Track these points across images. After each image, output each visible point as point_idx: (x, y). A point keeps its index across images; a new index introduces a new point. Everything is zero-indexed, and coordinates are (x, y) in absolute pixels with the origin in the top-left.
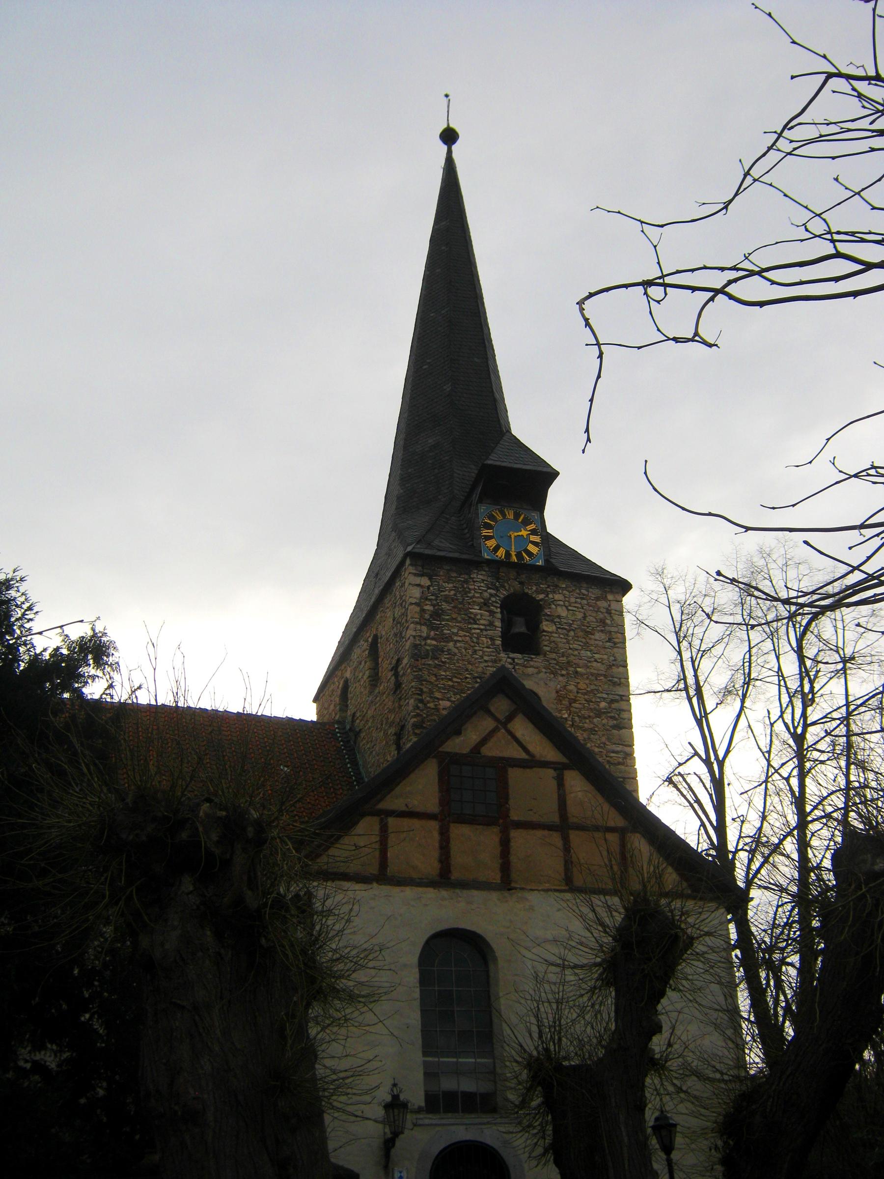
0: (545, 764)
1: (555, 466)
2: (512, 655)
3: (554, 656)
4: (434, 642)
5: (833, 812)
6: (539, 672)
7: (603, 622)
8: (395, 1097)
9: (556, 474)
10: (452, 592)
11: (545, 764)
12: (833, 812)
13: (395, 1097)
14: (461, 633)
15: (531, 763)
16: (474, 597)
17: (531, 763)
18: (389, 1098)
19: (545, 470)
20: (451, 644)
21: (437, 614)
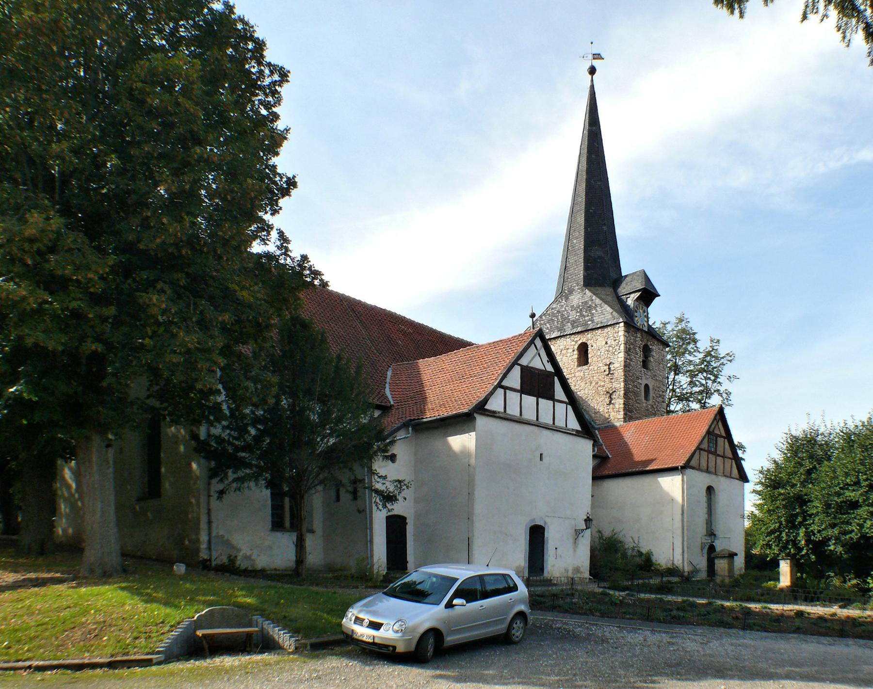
1: (659, 291)
15: (721, 436)
17: (721, 436)
21: (629, 349)
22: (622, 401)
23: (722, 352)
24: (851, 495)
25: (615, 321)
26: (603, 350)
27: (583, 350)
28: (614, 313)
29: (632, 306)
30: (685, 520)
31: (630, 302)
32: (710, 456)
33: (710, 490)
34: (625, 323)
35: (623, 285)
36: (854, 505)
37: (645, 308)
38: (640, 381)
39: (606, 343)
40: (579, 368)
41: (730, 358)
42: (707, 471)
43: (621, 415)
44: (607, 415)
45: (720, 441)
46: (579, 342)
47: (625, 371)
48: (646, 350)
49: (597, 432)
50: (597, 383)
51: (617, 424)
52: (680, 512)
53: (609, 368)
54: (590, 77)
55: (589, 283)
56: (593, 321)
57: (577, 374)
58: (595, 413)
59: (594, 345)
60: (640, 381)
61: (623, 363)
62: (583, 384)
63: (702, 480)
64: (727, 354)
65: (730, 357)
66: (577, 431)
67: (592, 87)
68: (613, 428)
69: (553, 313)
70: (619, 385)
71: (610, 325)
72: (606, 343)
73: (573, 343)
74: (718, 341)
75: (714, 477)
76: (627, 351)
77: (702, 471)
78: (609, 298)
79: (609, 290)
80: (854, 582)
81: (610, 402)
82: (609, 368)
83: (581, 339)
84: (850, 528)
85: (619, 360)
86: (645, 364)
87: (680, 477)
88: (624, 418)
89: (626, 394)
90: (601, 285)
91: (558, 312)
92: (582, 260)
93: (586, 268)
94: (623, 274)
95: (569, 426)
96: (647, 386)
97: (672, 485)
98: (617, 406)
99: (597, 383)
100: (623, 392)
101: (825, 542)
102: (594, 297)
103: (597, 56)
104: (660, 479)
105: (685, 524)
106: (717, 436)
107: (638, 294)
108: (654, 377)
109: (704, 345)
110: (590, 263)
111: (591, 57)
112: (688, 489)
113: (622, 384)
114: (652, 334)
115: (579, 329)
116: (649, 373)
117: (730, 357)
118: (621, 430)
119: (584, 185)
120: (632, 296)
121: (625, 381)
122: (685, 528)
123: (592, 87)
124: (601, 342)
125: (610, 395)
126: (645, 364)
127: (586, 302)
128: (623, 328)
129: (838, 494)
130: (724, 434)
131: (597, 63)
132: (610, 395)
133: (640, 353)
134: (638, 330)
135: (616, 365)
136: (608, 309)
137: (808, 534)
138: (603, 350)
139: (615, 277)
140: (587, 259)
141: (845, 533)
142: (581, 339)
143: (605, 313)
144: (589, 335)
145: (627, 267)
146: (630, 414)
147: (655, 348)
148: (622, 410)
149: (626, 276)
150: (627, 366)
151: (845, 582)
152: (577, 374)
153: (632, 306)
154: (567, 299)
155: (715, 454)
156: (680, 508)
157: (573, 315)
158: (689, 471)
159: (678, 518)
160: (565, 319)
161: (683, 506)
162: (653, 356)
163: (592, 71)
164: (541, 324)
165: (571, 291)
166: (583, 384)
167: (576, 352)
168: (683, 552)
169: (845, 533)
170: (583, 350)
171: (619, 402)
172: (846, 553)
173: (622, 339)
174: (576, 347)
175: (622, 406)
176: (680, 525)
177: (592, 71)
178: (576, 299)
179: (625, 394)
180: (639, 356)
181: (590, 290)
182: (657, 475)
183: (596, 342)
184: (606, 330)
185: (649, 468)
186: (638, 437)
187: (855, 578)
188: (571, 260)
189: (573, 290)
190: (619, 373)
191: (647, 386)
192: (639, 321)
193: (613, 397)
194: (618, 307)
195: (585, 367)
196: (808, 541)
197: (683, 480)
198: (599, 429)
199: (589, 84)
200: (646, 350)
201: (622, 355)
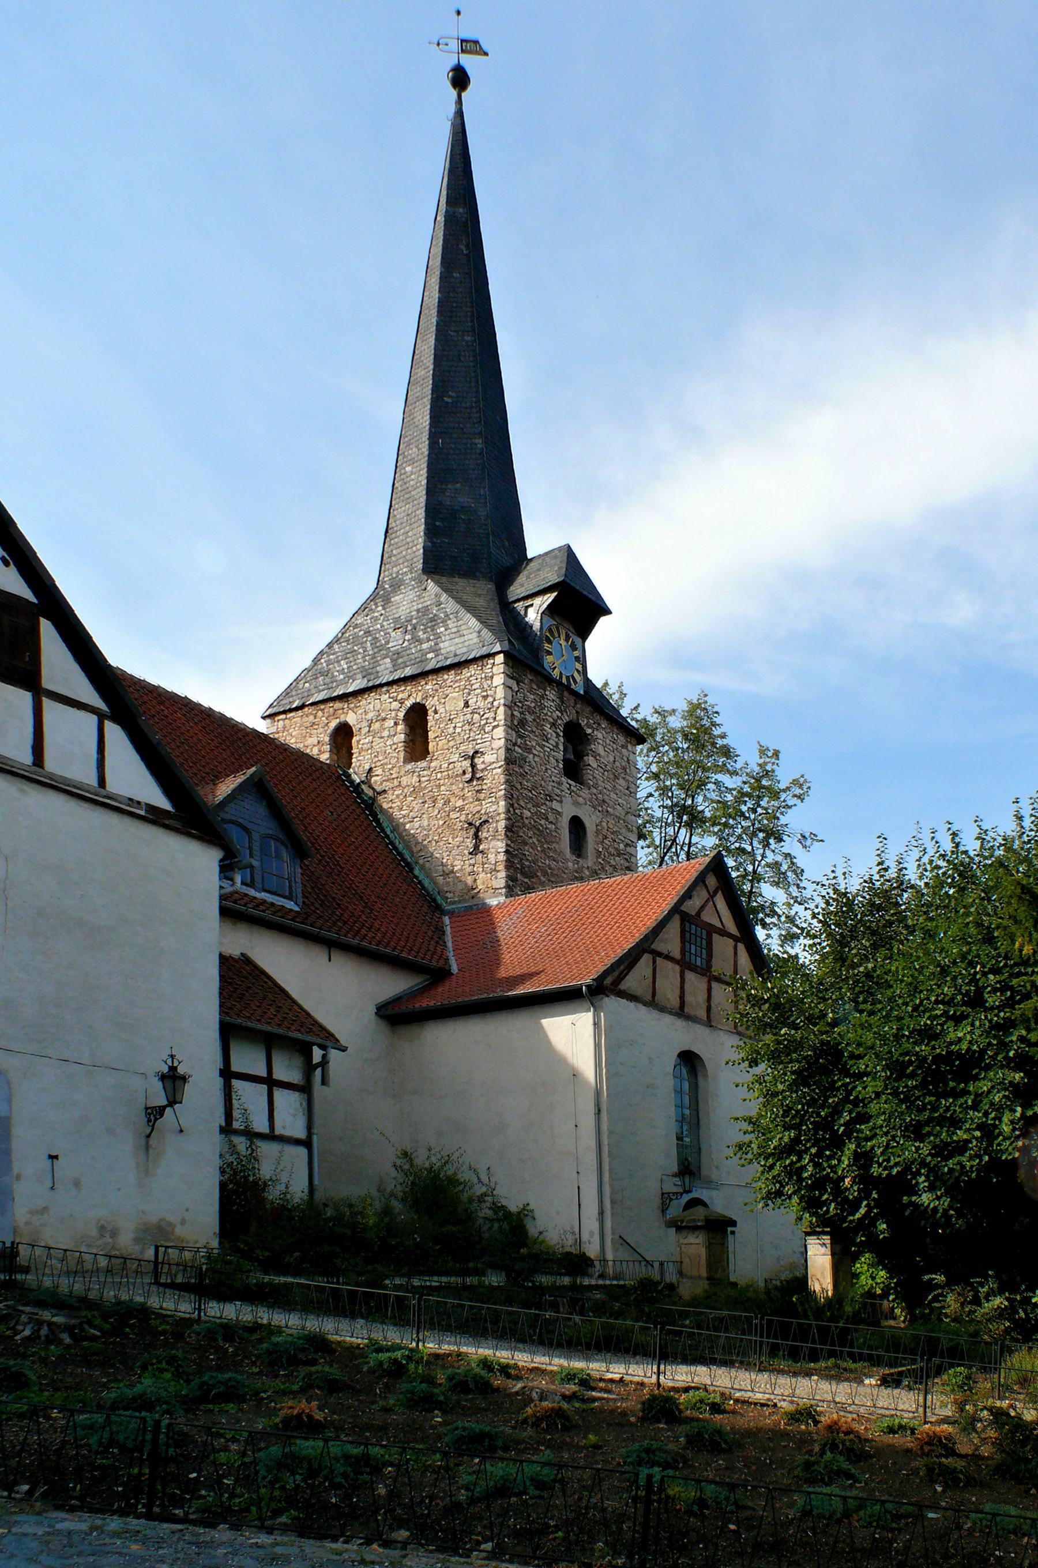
0: (730, 936)
1: (609, 601)
2: (570, 781)
3: (595, 791)
4: (520, 751)
5: (668, 957)
6: (586, 804)
7: (624, 769)
8: (173, 1069)
9: (607, 611)
10: (533, 705)
11: (730, 936)
12: (668, 957)
13: (173, 1069)
14: (538, 748)
15: (723, 933)
16: (546, 714)
17: (723, 933)
18: (165, 1069)
19: (593, 598)
20: (531, 756)
21: (522, 723)
22: (501, 845)
23: (784, 776)
24: (964, 1036)
25: (484, 651)
26: (459, 721)
27: (417, 719)
28: (485, 631)
29: (537, 626)
30: (605, 1127)
31: (533, 616)
32: (690, 976)
33: (689, 1060)
34: (507, 655)
35: (522, 578)
36: (969, 1065)
37: (578, 641)
38: (555, 805)
39: (467, 705)
40: (409, 767)
41: (798, 791)
42: (681, 1012)
43: (500, 880)
44: (469, 880)
45: (723, 946)
46: (408, 703)
47: (508, 772)
48: (576, 738)
49: (446, 920)
50: (447, 802)
51: (493, 902)
52: (591, 1109)
53: (473, 766)
54: (454, 93)
55: (439, 563)
56: (436, 650)
57: (405, 780)
58: (445, 874)
59: (441, 710)
60: (555, 805)
61: (502, 753)
62: (416, 805)
63: (669, 1035)
64: (795, 782)
65: (801, 787)
66: (151, 809)
67: (459, 114)
68: (485, 911)
69: (356, 636)
70: (496, 807)
71: (475, 660)
72: (467, 705)
73: (396, 705)
74: (776, 754)
75: (700, 1030)
76: (516, 725)
77: (662, 1009)
78: (481, 602)
79: (482, 590)
80: (998, 1301)
81: (476, 847)
82: (473, 766)
83: (412, 695)
84: (961, 1135)
85: (494, 744)
86: (573, 770)
87: (590, 1015)
88: (507, 887)
89: (510, 830)
90: (469, 574)
91: (368, 632)
92: (421, 513)
93: (431, 531)
94: (529, 556)
95: (114, 785)
96: (577, 825)
97: (572, 1036)
98: (492, 857)
99: (447, 802)
100: (502, 824)
101: (899, 1185)
102: (444, 596)
103: (471, 46)
104: (545, 1022)
105: (605, 1141)
106: (711, 929)
107: (550, 598)
108: (599, 804)
109: (748, 758)
110: (440, 520)
111: (455, 45)
112: (611, 1047)
113: (502, 803)
114: (595, 702)
115: (408, 671)
116: (585, 793)
117: (801, 787)
118: (497, 914)
119: (432, 341)
120: (537, 601)
121: (509, 797)
122: (605, 1150)
123: (459, 114)
124: (454, 701)
125: (476, 829)
126: (573, 770)
127: (426, 610)
128: (501, 668)
129: (927, 1035)
130: (731, 927)
131: (469, 62)
132: (476, 829)
133: (556, 739)
134: (546, 679)
135: (489, 758)
136: (473, 622)
137: (863, 1159)
138: (459, 721)
139: (507, 561)
140: (433, 511)
141: (945, 1151)
142: (412, 695)
143: (466, 633)
144: (429, 686)
145: (539, 539)
146: (522, 876)
147: (603, 742)
148: (501, 867)
149: (531, 559)
150: (512, 761)
151: (976, 1301)
152: (405, 780)
153: (537, 626)
154: (387, 601)
155: (706, 971)
156: (592, 1095)
157: (397, 640)
158: (611, 1003)
159: (588, 1122)
160: (380, 648)
161: (598, 1093)
162: (596, 755)
163: (460, 79)
164: (329, 662)
165: (397, 585)
166: (416, 805)
167: (401, 727)
168: (601, 1213)
169: (945, 1151)
170: (417, 719)
171: (496, 848)
172: (960, 1214)
173: (500, 693)
174: (401, 715)
175: (502, 857)
176: (593, 1143)
177: (460, 79)
178: (406, 603)
179: (508, 829)
180: (552, 750)
181: (437, 583)
182: (537, 1011)
183: (445, 701)
184: (466, 673)
185: (520, 990)
186: (529, 931)
187: (1001, 1292)
188: (399, 514)
189: (402, 581)
190: (495, 777)
191: (577, 825)
192: (556, 662)
193: (483, 834)
194: (496, 619)
195: (423, 764)
196: (866, 1181)
197: (596, 1024)
198: (451, 914)
199: (452, 109)
200: (576, 738)
201: (500, 733)
